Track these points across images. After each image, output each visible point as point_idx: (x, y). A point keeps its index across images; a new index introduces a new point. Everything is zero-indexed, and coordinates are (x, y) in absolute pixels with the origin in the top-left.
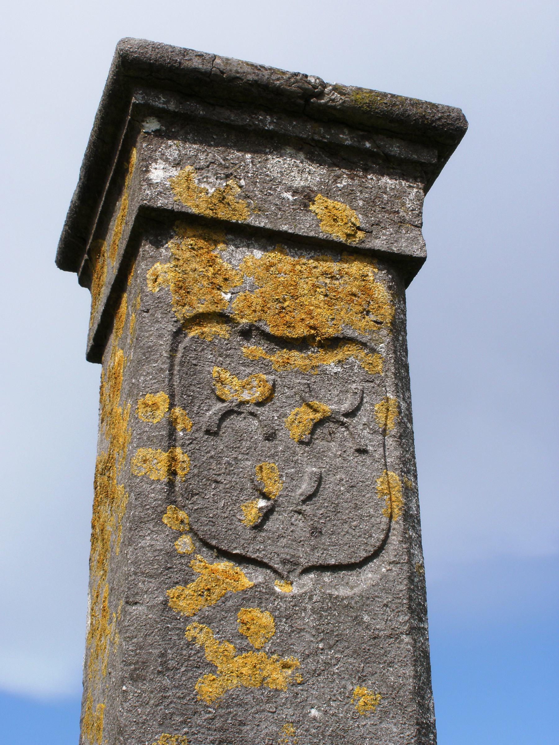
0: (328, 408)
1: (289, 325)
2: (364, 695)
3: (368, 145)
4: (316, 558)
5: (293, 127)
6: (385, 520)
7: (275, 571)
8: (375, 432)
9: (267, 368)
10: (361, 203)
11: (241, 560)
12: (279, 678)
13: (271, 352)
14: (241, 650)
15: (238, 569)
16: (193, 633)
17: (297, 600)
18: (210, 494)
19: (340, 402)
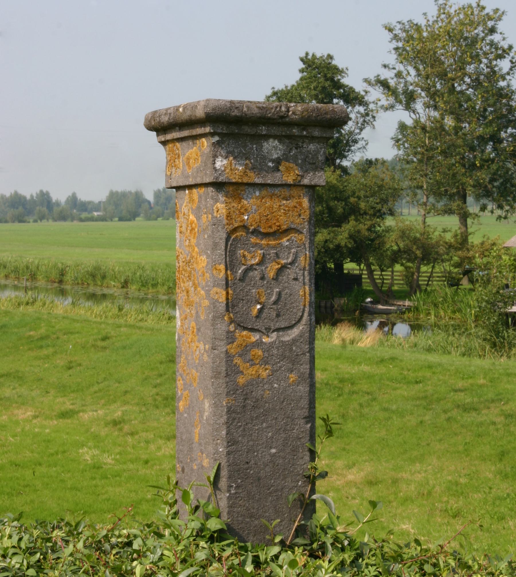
0: (283, 262)
1: (270, 227)
2: (293, 377)
3: (305, 133)
4: (278, 325)
5: (275, 130)
6: (302, 307)
7: (263, 333)
8: (300, 270)
9: (261, 248)
10: (300, 161)
11: (252, 330)
12: (264, 374)
13: (262, 239)
14: (252, 365)
15: (250, 333)
16: (236, 361)
17: (272, 344)
18: (240, 305)
19: (288, 258)
